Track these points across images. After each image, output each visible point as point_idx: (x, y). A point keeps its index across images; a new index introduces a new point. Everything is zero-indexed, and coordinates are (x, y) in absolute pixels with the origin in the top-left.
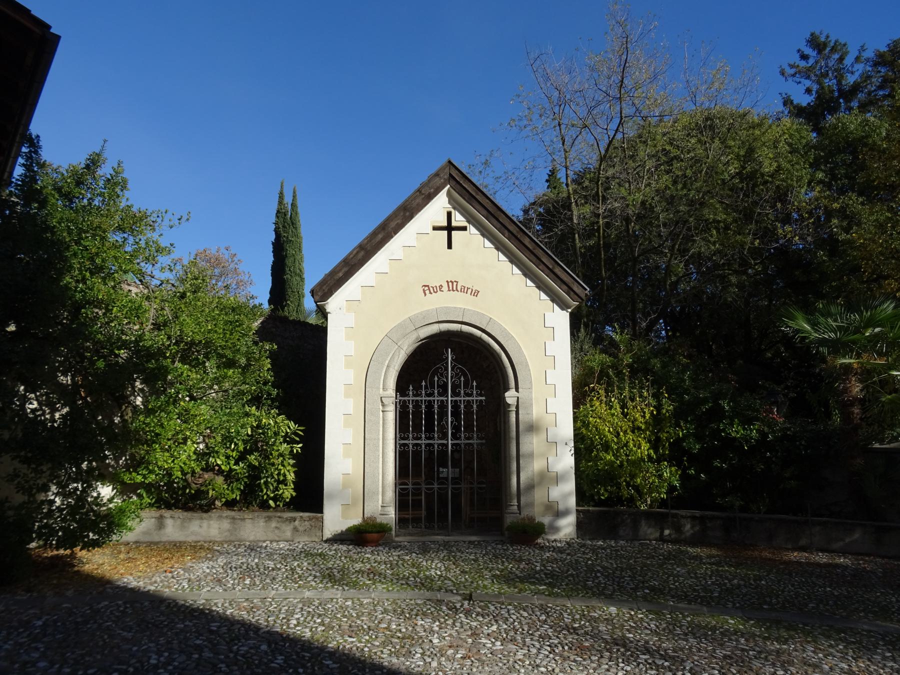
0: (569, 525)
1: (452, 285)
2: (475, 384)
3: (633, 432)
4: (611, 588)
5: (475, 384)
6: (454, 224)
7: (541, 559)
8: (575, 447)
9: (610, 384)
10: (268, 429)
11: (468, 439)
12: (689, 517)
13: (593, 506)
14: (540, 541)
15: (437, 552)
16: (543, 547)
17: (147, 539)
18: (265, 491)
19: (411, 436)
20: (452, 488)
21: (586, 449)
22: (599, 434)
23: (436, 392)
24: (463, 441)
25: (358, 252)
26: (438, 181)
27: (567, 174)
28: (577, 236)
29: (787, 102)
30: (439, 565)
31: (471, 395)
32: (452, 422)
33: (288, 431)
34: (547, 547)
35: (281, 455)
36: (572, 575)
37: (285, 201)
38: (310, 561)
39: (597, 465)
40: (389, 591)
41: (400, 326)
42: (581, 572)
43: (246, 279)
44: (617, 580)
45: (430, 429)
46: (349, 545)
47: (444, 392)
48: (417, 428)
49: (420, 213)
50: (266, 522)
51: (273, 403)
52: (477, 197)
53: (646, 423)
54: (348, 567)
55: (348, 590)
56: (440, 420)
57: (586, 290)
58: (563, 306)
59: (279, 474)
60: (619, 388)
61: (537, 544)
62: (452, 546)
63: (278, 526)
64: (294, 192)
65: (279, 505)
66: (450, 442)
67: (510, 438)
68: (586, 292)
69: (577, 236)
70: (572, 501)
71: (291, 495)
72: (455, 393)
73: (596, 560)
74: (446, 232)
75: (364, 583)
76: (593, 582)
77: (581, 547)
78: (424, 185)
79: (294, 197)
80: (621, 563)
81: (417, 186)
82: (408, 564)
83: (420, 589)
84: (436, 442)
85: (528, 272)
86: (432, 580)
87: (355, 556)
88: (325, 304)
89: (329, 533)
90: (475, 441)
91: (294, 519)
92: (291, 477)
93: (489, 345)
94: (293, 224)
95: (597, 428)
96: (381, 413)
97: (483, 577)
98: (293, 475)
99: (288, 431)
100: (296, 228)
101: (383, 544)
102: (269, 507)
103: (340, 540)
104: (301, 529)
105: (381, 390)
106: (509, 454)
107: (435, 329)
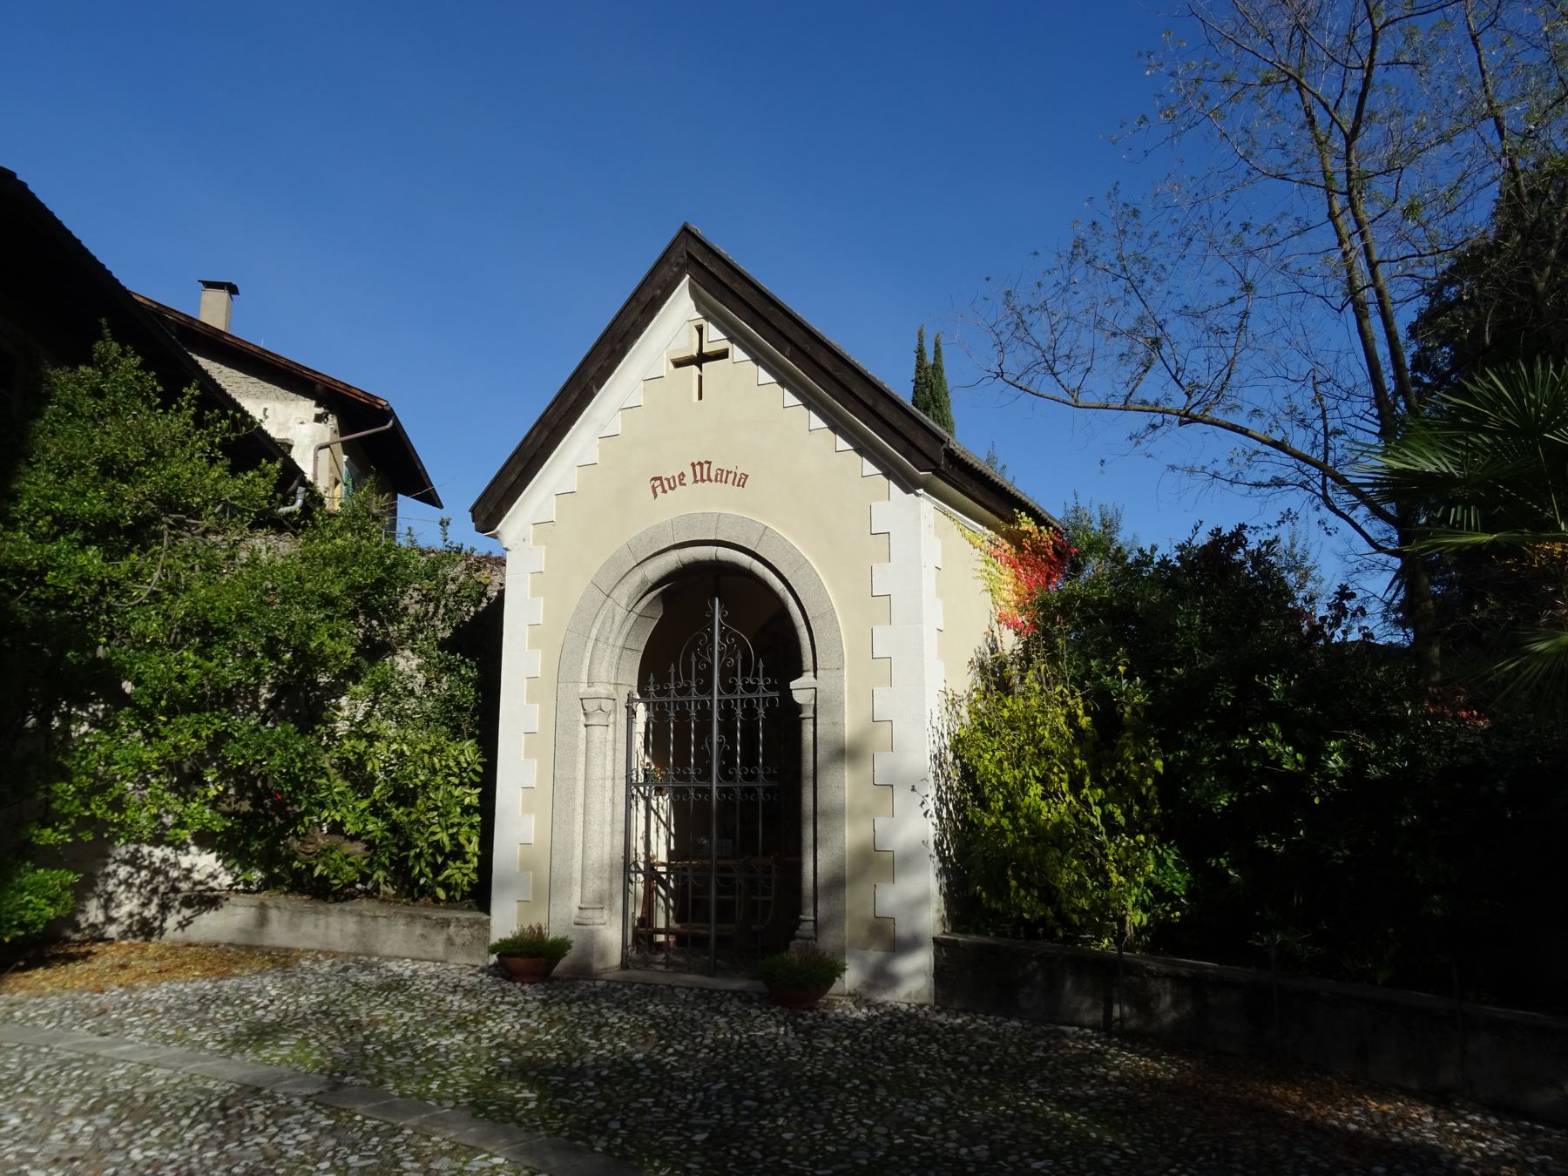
0: (918, 972)
1: (702, 471)
2: (761, 665)
12: (1166, 976)
17: (241, 940)
25: (540, 432)
32: (720, 744)
50: (407, 924)
66: (715, 785)
94: (935, 400)
104: (458, 941)
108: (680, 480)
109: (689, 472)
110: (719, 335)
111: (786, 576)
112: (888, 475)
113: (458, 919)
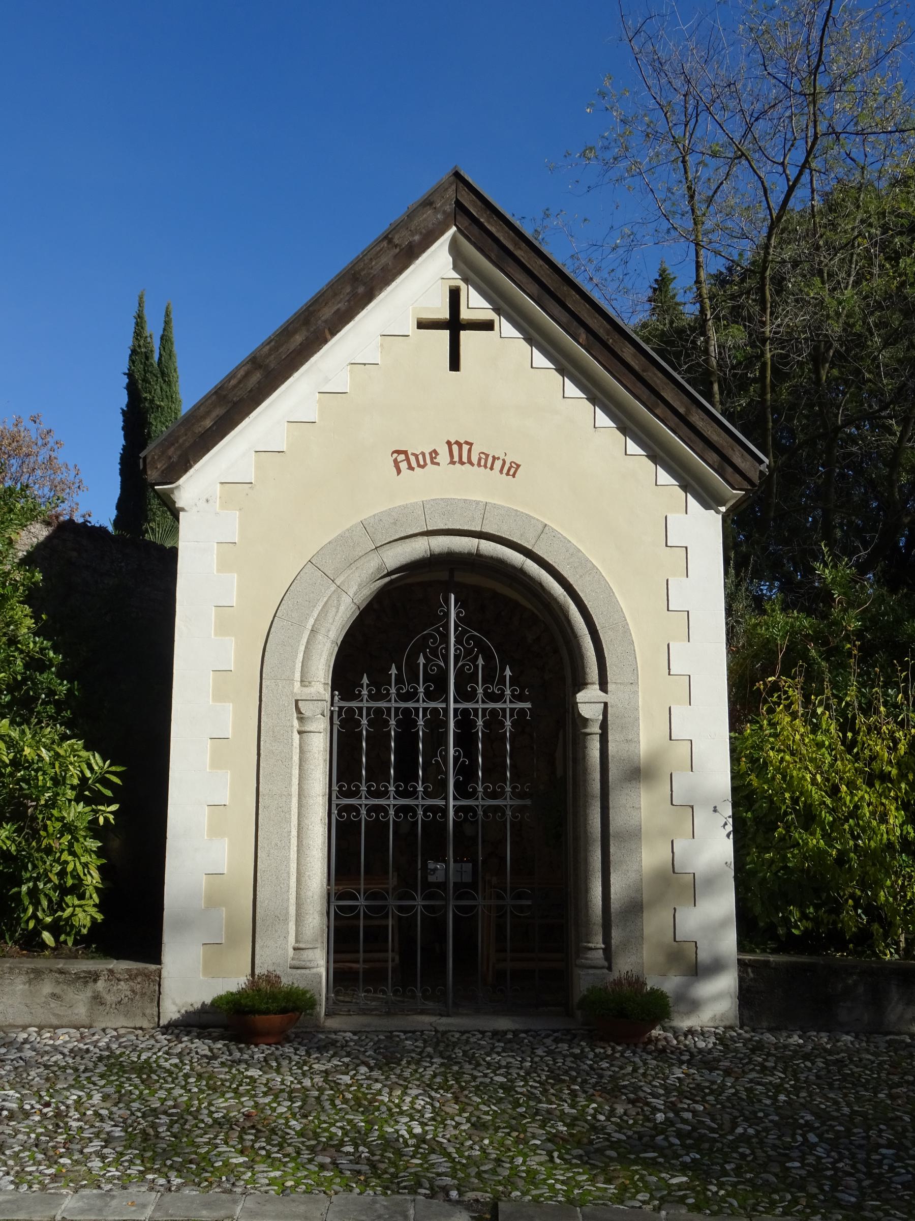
2: (508, 672)
3: (871, 784)
4: (851, 1181)
5: (508, 672)
7: (664, 1086)
8: (735, 817)
9: (812, 676)
10: (37, 771)
11: (494, 795)
13: (774, 951)
14: (656, 1032)
15: (418, 1063)
16: (664, 1050)
18: (31, 910)
19: (364, 788)
20: (457, 907)
21: (757, 820)
22: (790, 788)
23: (421, 689)
24: (480, 802)
25: (247, 375)
26: (429, 217)
27: (697, 262)
28: (716, 387)
30: (419, 1104)
31: (499, 698)
32: (456, 759)
33: (88, 774)
34: (677, 1051)
35: (68, 828)
36: (744, 1138)
37: (147, 333)
38: (110, 1090)
39: (784, 858)
40: (284, 1190)
41: (342, 540)
42: (766, 1130)
43: (71, 478)
44: (862, 1155)
45: (406, 773)
46: (215, 1040)
47: (438, 690)
48: (378, 771)
49: (389, 289)
50: (30, 982)
51: (58, 712)
52: (518, 253)
53: (899, 765)
54: (199, 1110)
55: (179, 1188)
57: (761, 462)
58: (709, 499)
59: (62, 874)
60: (834, 685)
61: (650, 1041)
62: (455, 1045)
63: (57, 991)
64: (167, 315)
65: (65, 942)
66: (452, 803)
67: (586, 795)
68: (763, 467)
69: (716, 387)
71: (93, 920)
72: (464, 694)
73: (797, 1089)
74: (445, 334)
75: (226, 1164)
76: (802, 1160)
77: (753, 1051)
78: (396, 228)
79: (167, 323)
80: (859, 1099)
81: (381, 228)
82: (345, 1101)
83: (366, 1184)
84: (421, 802)
85: (628, 423)
86: (399, 1153)
87: (223, 1074)
88: (172, 490)
89: (174, 1009)
90: (509, 802)
91: (94, 977)
92: (93, 879)
93: (540, 585)
94: (163, 374)
95: (784, 778)
96: (296, 737)
97: (526, 1142)
98: (95, 874)
99: (88, 774)
100: (169, 384)
101: (297, 1036)
102: (43, 946)
104: (110, 999)
105: (297, 685)
106: (586, 832)
107: (419, 548)
108: (432, 459)
109: (443, 451)
110: (482, 303)
111: (571, 580)
112: (685, 487)
113: (111, 971)
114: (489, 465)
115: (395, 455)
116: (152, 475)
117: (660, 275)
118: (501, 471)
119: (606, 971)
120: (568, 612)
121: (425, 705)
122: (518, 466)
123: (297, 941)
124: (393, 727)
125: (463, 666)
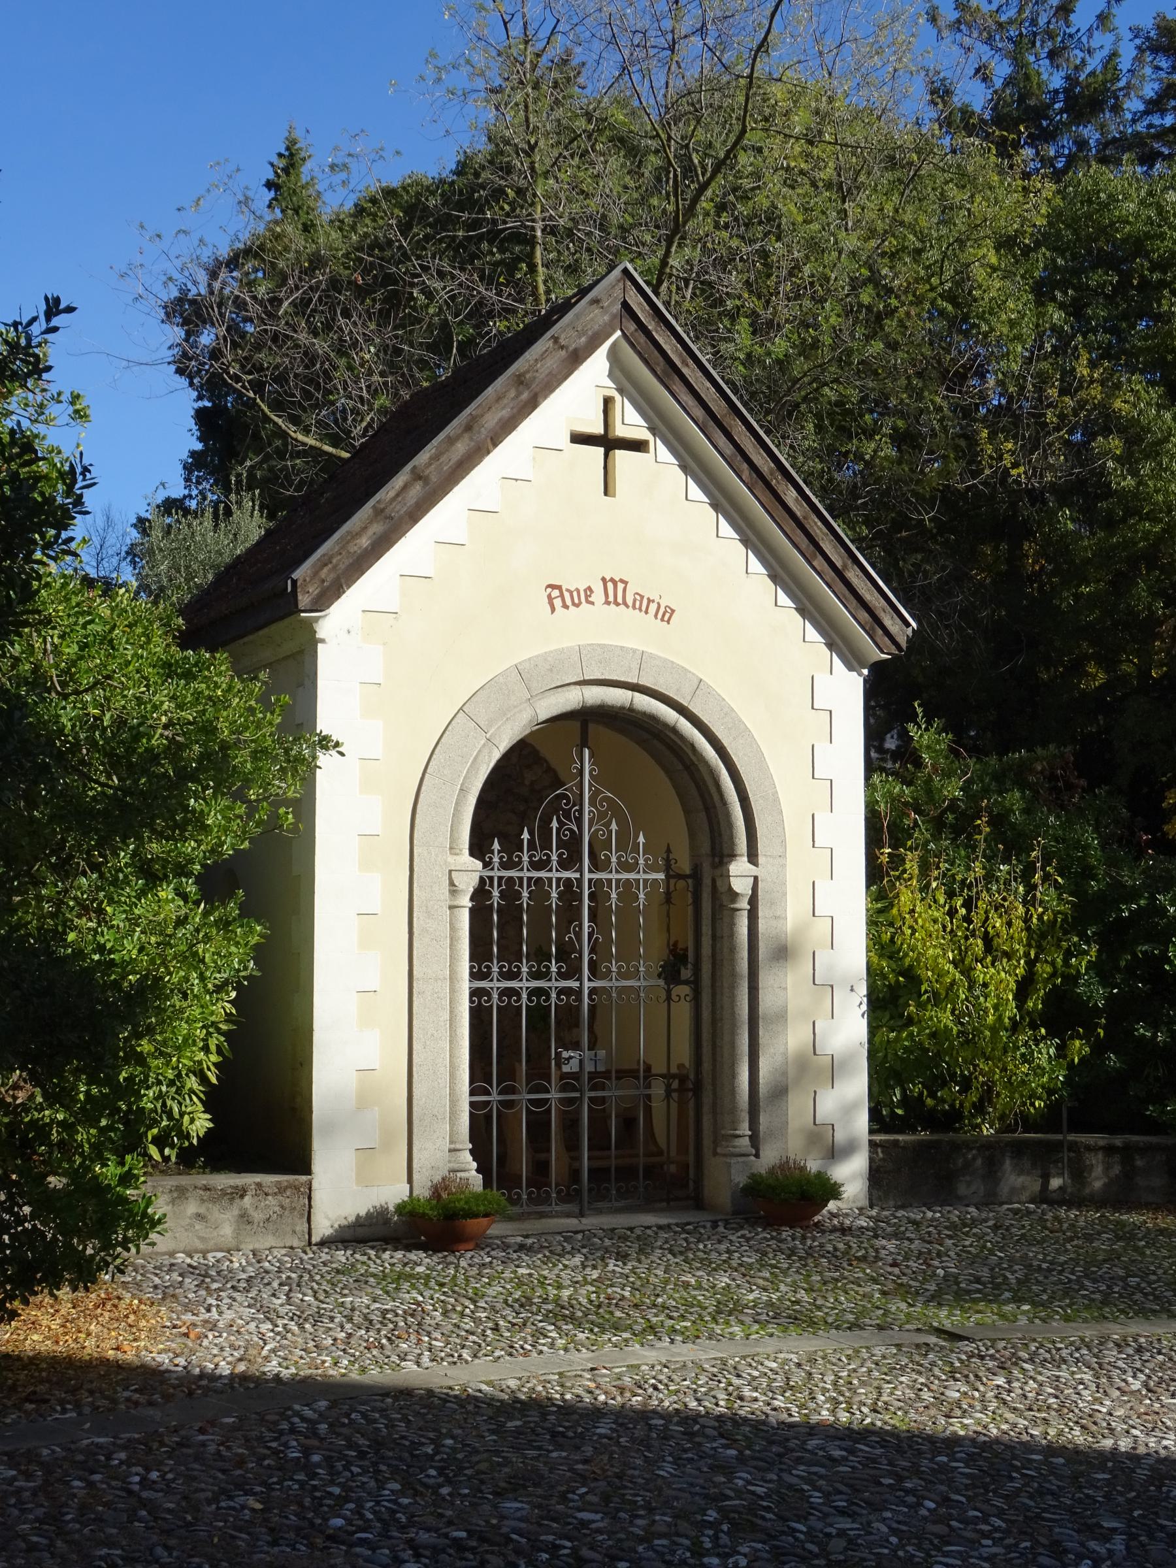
0: (854, 1177)
2: (641, 839)
5: (641, 839)
6: (620, 431)
23: (554, 857)
29: (940, 93)
32: (590, 935)
52: (685, 371)
56: (563, 929)
57: (908, 625)
58: (852, 659)
63: (202, 1210)
67: (734, 975)
70: (862, 1121)
88: (317, 619)
89: (327, 1223)
91: (242, 1192)
93: (692, 746)
103: (343, 1241)
104: (258, 1216)
108: (587, 597)
109: (598, 588)
111: (726, 742)
113: (259, 1185)
114: (644, 608)
115: (549, 590)
116: (304, 600)
117: (288, 149)
118: (656, 616)
119: (753, 1158)
120: (719, 777)
121: (559, 875)
122: (673, 611)
123: (451, 1142)
124: (525, 900)
125: (597, 831)
